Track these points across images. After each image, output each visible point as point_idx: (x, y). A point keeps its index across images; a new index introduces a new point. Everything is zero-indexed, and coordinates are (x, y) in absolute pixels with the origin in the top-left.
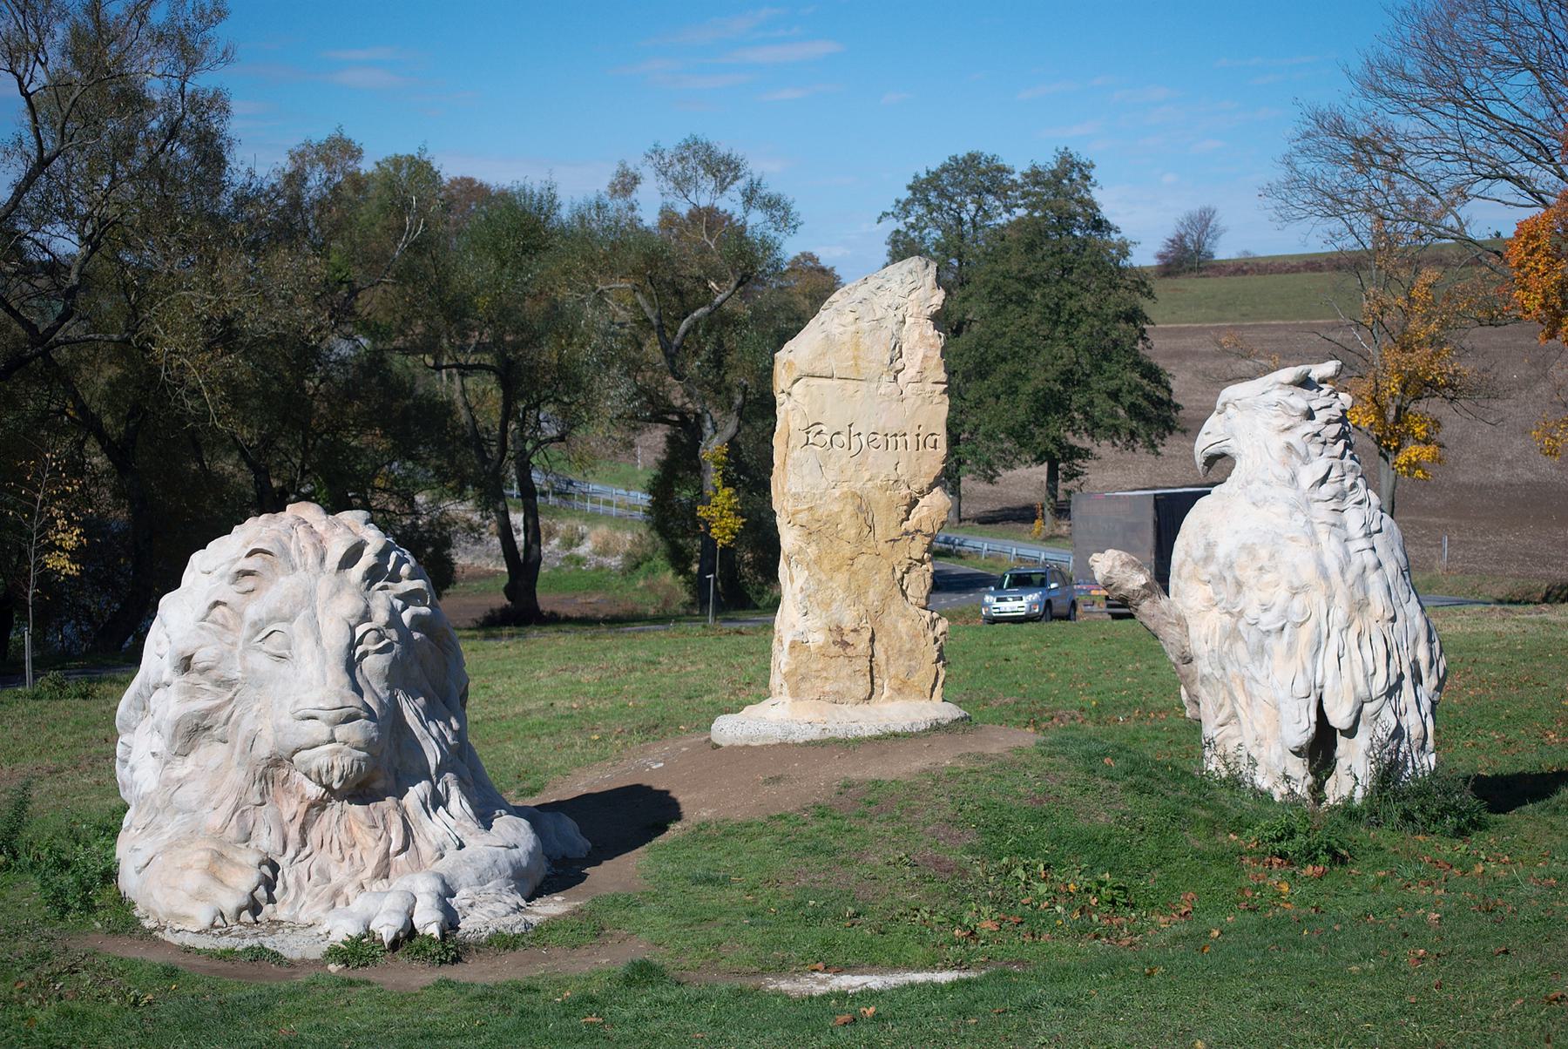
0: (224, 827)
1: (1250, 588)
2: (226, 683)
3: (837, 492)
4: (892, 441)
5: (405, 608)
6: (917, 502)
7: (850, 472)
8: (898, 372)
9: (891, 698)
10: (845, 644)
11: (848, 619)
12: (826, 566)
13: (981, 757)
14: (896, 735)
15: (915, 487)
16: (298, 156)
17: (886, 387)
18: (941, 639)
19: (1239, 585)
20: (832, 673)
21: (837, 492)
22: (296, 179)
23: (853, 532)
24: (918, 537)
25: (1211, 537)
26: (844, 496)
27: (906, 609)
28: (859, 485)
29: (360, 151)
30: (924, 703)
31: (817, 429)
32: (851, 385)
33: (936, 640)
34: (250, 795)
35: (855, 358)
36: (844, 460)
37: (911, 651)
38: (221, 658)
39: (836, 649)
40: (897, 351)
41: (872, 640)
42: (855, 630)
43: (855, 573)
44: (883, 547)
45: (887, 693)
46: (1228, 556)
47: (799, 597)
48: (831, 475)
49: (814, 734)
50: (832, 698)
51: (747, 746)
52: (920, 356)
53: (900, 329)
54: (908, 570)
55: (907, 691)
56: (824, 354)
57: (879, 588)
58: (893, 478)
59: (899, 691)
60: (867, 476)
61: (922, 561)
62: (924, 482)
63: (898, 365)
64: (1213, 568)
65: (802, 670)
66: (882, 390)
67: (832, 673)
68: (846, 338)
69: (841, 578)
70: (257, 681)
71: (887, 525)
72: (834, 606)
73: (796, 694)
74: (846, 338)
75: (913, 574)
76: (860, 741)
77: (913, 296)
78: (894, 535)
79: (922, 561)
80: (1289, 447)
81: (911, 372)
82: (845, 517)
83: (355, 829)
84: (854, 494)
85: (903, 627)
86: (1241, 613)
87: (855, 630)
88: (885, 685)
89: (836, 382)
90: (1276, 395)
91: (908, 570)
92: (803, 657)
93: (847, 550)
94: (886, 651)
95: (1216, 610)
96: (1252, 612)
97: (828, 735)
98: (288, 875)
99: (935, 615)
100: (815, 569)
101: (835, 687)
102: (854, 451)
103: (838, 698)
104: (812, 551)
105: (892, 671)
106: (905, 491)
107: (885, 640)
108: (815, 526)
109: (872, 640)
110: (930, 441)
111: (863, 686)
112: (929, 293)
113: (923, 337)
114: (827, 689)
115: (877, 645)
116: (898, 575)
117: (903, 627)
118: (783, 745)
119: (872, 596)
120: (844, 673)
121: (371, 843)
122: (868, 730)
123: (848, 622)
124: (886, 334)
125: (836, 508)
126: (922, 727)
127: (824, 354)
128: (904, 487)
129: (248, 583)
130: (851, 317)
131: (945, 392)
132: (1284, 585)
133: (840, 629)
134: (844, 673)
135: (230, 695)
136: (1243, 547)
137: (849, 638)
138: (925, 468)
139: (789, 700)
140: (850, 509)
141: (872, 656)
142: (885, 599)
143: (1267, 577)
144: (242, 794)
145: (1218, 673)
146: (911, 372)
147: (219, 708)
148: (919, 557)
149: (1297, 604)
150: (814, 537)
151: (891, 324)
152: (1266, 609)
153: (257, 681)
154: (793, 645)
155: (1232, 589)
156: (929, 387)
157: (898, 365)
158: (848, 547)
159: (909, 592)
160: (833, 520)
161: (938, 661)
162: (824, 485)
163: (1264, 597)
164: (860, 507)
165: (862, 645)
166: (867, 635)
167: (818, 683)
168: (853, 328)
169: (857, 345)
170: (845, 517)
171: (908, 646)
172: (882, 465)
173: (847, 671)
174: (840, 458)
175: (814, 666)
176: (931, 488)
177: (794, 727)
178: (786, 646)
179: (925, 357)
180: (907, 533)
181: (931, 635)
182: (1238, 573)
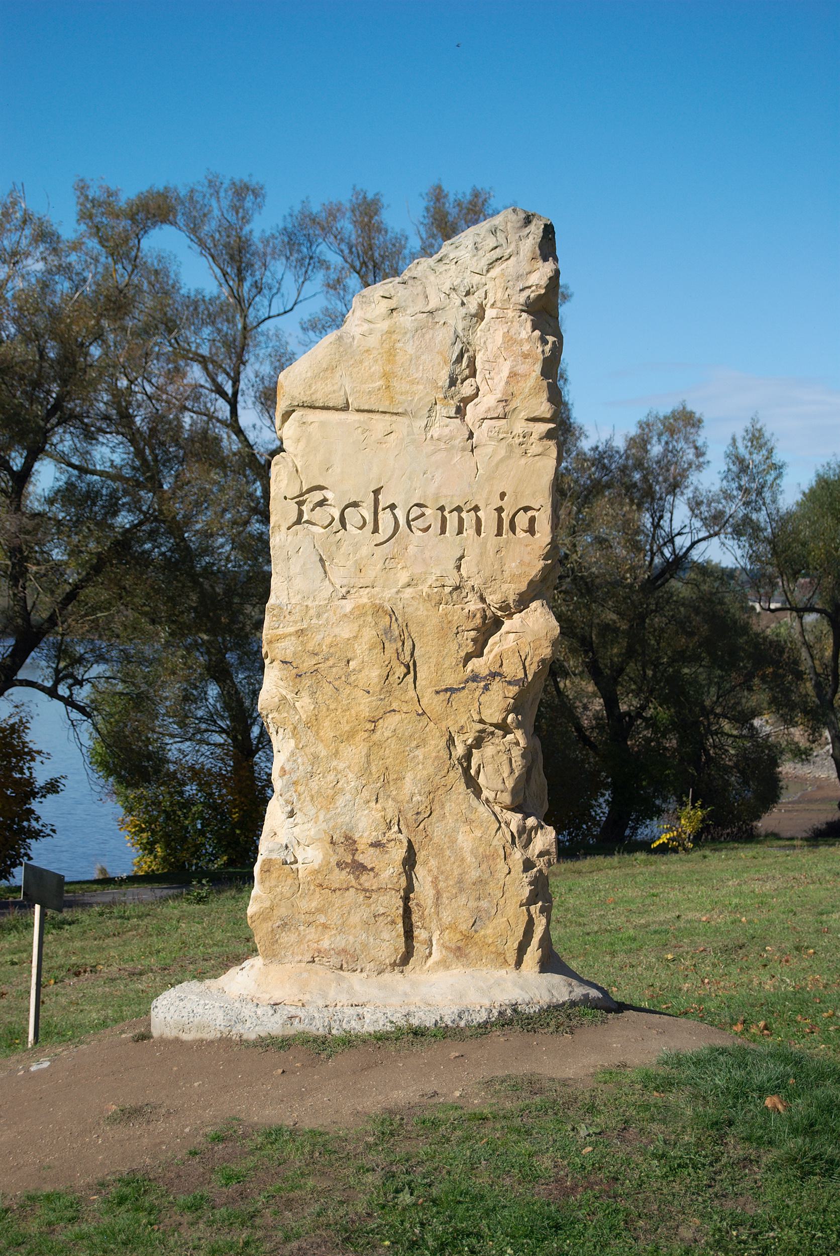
3: (348, 606)
4: (452, 520)
6: (497, 624)
7: (372, 572)
8: (466, 401)
9: (444, 964)
10: (359, 868)
11: (366, 824)
12: (327, 731)
13: (533, 1085)
14: (418, 1033)
15: (493, 599)
16: (645, 426)
17: (444, 426)
18: (541, 864)
20: (334, 918)
21: (348, 606)
22: (640, 443)
23: (374, 674)
26: (359, 613)
27: (473, 810)
28: (388, 593)
29: (700, 421)
30: (507, 974)
31: (317, 496)
32: (380, 423)
33: (528, 865)
35: (385, 375)
36: (364, 551)
37: (480, 882)
39: (340, 877)
40: (465, 363)
41: (410, 862)
42: (376, 845)
43: (379, 745)
44: (432, 702)
45: (436, 955)
48: (339, 575)
49: (273, 1026)
50: (335, 961)
51: (177, 1040)
52: (505, 373)
53: (470, 328)
54: (478, 743)
55: (473, 952)
56: (331, 369)
57: (423, 773)
58: (453, 580)
59: (459, 952)
60: (403, 577)
61: (503, 727)
62: (511, 590)
63: (466, 389)
65: (283, 911)
66: (435, 431)
67: (334, 918)
68: (373, 341)
71: (438, 662)
72: (341, 801)
75: (489, 750)
76: (348, 1042)
77: (496, 272)
78: (452, 679)
79: (503, 727)
81: (487, 401)
82: (361, 649)
84: (378, 610)
85: (465, 840)
87: (376, 845)
88: (433, 934)
89: (351, 417)
91: (478, 743)
92: (285, 888)
93: (364, 705)
94: (435, 882)
97: (298, 1027)
99: (531, 821)
101: (340, 942)
102: (382, 536)
103: (347, 961)
104: (304, 704)
105: (446, 917)
106: (474, 605)
107: (433, 863)
108: (308, 663)
109: (410, 862)
110: (522, 520)
111: (390, 941)
112: (525, 267)
113: (510, 340)
114: (325, 944)
115: (420, 871)
116: (460, 750)
117: (465, 840)
118: (225, 1043)
119: (411, 786)
120: (355, 919)
122: (373, 1021)
124: (443, 336)
125: (345, 632)
126: (482, 1017)
127: (331, 369)
128: (473, 598)
131: (549, 435)
133: (350, 842)
134: (355, 919)
137: (367, 857)
138: (512, 566)
139: (343, 202)
140: (369, 634)
141: (410, 888)
142: (433, 794)
146: (487, 401)
148: (497, 718)
150: (307, 682)
151: (455, 317)
156: (520, 426)
157: (466, 389)
159: (482, 780)
161: (531, 901)
162: (326, 594)
164: (388, 631)
165: (389, 867)
166: (398, 853)
167: (311, 933)
168: (384, 325)
169: (391, 354)
170: (361, 649)
171: (474, 874)
172: (431, 557)
173: (363, 913)
174: (356, 546)
175: (304, 905)
176: (523, 602)
177: (247, 1011)
179: (513, 375)
180: (475, 678)
181: (517, 855)
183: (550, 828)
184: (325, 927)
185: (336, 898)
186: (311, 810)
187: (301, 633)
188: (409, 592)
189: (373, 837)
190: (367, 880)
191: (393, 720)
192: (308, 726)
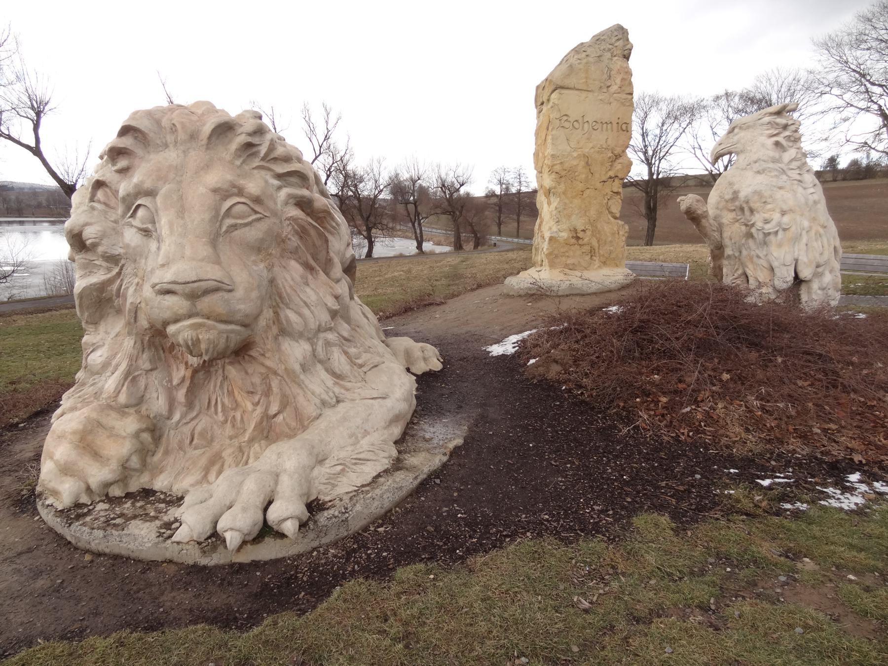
0: (118, 392)
1: (758, 212)
2: (112, 259)
5: (279, 188)
10: (578, 238)
19: (752, 211)
24: (616, 180)
25: (736, 187)
26: (579, 156)
32: (584, 94)
34: (140, 362)
35: (586, 78)
38: (103, 236)
39: (573, 241)
44: (599, 185)
46: (746, 197)
47: (554, 213)
48: (573, 144)
59: (604, 263)
64: (737, 203)
65: (556, 252)
67: (571, 253)
69: (577, 201)
70: (135, 255)
73: (552, 265)
74: (581, 66)
78: (604, 178)
80: (777, 144)
82: (580, 168)
83: (236, 393)
84: (584, 155)
86: (753, 225)
87: (583, 231)
90: (767, 119)
93: (581, 186)
95: (737, 224)
96: (759, 224)
98: (172, 437)
100: (563, 196)
104: (562, 188)
114: (568, 262)
119: (593, 213)
121: (250, 407)
123: (580, 227)
125: (575, 163)
129: (122, 163)
130: (584, 54)
132: (778, 210)
133: (575, 230)
135: (117, 270)
136: (755, 192)
137: (581, 235)
139: (547, 268)
140: (582, 163)
143: (769, 207)
144: (133, 360)
145: (737, 254)
147: (110, 281)
149: (786, 219)
150: (563, 179)
152: (767, 222)
153: (135, 255)
154: (551, 239)
155: (747, 213)
158: (581, 185)
160: (572, 170)
163: (767, 216)
167: (564, 259)
168: (585, 61)
173: (579, 253)
175: (562, 250)
178: (547, 240)
180: (611, 178)
182: (752, 205)
183: (640, 521)
184: (568, 257)
185: (573, 248)
186: (564, 220)
187: (561, 163)
188: (592, 150)
189: (583, 228)
190: (580, 242)
191: (588, 191)
192: (564, 193)
